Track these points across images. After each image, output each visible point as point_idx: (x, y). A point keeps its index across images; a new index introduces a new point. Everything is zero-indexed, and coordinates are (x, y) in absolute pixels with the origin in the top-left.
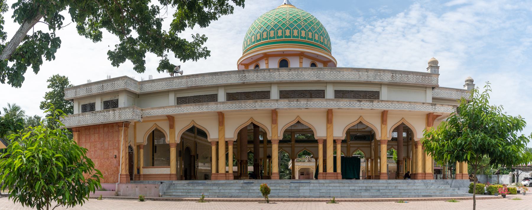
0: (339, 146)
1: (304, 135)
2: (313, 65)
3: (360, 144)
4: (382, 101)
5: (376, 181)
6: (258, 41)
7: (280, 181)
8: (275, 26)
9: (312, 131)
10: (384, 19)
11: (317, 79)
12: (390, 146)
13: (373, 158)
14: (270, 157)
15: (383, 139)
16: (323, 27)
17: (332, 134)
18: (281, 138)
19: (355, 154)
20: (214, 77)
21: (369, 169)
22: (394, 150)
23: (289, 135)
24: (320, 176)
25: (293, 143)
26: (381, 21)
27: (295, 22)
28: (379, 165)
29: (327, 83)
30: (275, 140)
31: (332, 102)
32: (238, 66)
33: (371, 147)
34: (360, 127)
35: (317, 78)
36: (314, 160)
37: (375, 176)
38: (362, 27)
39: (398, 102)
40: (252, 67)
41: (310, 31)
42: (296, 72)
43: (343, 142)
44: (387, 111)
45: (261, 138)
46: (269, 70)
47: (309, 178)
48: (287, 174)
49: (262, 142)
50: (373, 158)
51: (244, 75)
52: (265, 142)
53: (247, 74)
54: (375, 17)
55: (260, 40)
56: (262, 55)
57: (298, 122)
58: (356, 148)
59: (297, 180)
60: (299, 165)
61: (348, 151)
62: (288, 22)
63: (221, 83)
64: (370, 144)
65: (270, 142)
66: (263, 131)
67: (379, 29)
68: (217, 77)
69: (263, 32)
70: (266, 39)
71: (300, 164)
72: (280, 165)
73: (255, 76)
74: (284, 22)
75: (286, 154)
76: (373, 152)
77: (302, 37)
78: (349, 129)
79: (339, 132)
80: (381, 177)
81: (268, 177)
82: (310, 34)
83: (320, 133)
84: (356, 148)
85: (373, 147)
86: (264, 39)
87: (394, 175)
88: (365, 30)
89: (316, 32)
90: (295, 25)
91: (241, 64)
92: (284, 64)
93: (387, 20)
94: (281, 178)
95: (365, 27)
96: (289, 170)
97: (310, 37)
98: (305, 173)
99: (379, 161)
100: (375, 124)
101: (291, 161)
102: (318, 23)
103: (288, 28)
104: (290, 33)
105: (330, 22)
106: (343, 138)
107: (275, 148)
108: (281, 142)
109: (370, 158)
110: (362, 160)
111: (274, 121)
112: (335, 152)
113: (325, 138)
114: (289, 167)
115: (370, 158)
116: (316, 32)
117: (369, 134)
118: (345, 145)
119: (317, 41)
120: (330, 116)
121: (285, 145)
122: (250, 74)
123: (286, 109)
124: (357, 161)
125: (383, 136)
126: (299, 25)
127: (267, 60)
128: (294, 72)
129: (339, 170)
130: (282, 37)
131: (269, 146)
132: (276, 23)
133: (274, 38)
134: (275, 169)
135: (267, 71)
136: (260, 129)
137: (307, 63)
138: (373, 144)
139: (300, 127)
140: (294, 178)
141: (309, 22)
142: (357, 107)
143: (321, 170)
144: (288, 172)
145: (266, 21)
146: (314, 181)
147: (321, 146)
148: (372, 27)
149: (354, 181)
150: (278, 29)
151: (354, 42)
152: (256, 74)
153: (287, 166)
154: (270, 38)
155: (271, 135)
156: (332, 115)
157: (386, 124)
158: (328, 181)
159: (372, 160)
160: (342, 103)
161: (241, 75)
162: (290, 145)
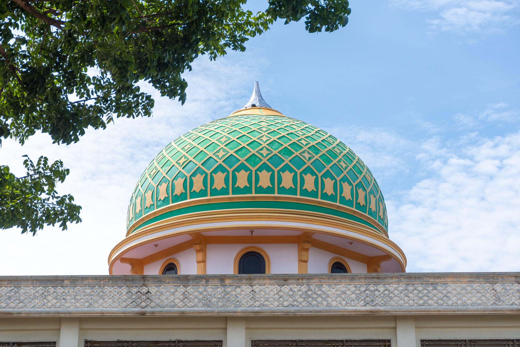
2: (338, 268)
6: (176, 198)
8: (229, 159)
10: (498, 138)
11: (368, 308)
16: (363, 166)
20: (52, 290)
26: (491, 143)
27: (287, 151)
29: (395, 319)
32: (111, 265)
35: (367, 304)
38: (437, 164)
40: (154, 270)
41: (328, 174)
42: (304, 288)
46: (310, 277)
51: (145, 290)
53: (153, 289)
54: (473, 135)
55: (183, 196)
56: (188, 238)
62: (264, 152)
63: (72, 309)
67: (487, 166)
68: (60, 290)
69: (194, 174)
70: (203, 193)
73: (178, 294)
74: (253, 152)
77: (305, 192)
82: (329, 183)
86: (194, 194)
88: (445, 171)
89: (344, 179)
90: (287, 160)
91: (122, 258)
92: (252, 264)
93: (507, 139)
95: (445, 162)
97: (329, 189)
102: (350, 156)
103: (265, 167)
104: (272, 179)
105: (374, 150)
116: (344, 179)
119: (350, 203)
122: (162, 289)
126: (298, 161)
127: (203, 250)
128: (295, 288)
130: (247, 190)
132: (232, 152)
133: (225, 191)
135: (216, 282)
137: (319, 263)
141: (324, 151)
145: (201, 148)
148: (467, 162)
150: (238, 169)
151: (416, 204)
152: (182, 289)
154: (214, 192)
161: (135, 290)
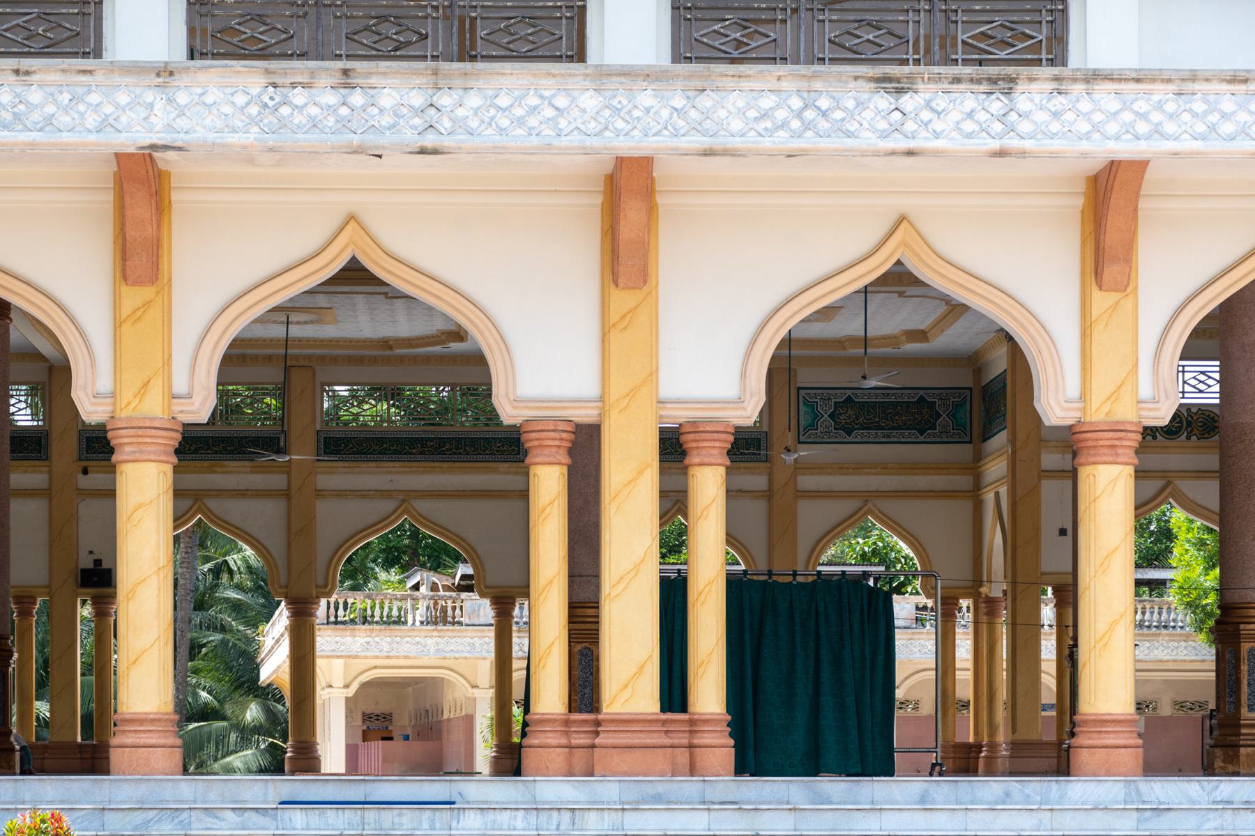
0: (709, 485)
1: (392, 393)
3: (883, 468)
4: (1093, 77)
5: (1035, 787)
7: (188, 789)
9: (478, 360)
12: (1156, 484)
13: (996, 589)
14: (99, 580)
15: (1097, 413)
17: (653, 375)
18: (200, 406)
19: (842, 556)
21: (964, 686)
22: (1178, 517)
23: (258, 390)
24: (543, 748)
25: (301, 455)
28: (1048, 648)
30: (142, 427)
31: (647, 98)
33: (975, 494)
34: (891, 319)
36: (480, 608)
37: (1017, 747)
39: (1237, 79)
43: (746, 447)
44: (1139, 167)
45: (23, 415)
47: (435, 766)
48: (247, 734)
49: (29, 445)
50: (996, 589)
52: (64, 449)
57: (354, 275)
58: (849, 506)
59: (334, 778)
60: (349, 658)
61: (780, 526)
64: (974, 468)
65: (97, 446)
66: (44, 347)
71: (358, 641)
72: (187, 650)
75: (234, 560)
76: (995, 541)
78: (788, 342)
79: (714, 367)
80: (1082, 757)
81: (89, 757)
83: (542, 367)
84: (849, 506)
85: (996, 493)
87: (1192, 741)
94: (196, 758)
96: (267, 694)
98: (403, 722)
99: (1048, 613)
100: (1023, 281)
101: (282, 618)
106: (748, 413)
107: (144, 497)
108: (195, 446)
109: (974, 588)
110: (903, 607)
111: (139, 256)
112: (673, 543)
113: (585, 415)
114: (265, 674)
115: (974, 588)
117: (964, 379)
118: (756, 480)
120: (632, 213)
121: (232, 475)
123: (246, 156)
124: (859, 614)
125: (1101, 387)
129: (709, 691)
131: (95, 480)
134: (145, 679)
136: (18, 332)
138: (996, 468)
139: (360, 322)
140: (307, 761)
142: (868, 140)
143: (551, 695)
144: (253, 713)
146: (486, 788)
147: (549, 483)
149: (833, 786)
153: (244, 677)
155: (104, 382)
156: (651, 208)
157: (1125, 284)
158: (609, 789)
159: (987, 609)
160: (736, 100)
162: (277, 481)
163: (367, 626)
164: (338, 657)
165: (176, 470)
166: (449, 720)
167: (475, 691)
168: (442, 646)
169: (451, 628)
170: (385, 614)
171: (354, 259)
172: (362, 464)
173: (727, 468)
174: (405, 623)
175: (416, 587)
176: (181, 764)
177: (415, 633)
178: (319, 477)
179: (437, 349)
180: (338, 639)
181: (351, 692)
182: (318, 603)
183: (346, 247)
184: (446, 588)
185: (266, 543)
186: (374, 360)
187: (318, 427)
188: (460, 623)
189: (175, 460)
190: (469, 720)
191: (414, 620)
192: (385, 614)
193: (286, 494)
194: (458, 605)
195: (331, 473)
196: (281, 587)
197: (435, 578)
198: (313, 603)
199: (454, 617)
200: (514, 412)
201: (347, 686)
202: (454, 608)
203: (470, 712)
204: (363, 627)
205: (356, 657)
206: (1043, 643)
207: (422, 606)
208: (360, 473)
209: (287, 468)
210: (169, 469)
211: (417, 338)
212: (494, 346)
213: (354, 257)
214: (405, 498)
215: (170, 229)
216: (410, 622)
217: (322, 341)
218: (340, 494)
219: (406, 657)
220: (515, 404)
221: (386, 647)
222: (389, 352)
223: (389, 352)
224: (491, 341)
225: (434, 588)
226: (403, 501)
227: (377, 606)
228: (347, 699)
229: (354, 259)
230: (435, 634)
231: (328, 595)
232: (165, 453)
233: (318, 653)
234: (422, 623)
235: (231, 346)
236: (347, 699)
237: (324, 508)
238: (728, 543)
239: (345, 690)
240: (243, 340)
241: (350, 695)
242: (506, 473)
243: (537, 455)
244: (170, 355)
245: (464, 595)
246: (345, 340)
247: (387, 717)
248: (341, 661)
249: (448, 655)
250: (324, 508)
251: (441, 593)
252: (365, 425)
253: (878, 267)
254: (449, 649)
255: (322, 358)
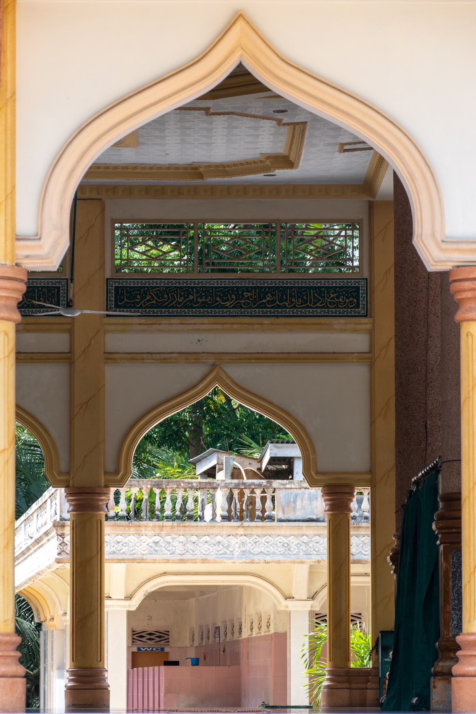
98: (182, 643)
163: (155, 523)
164: (119, 561)
165: (20, 329)
166: (248, 640)
167: (289, 603)
168: (248, 547)
169: (261, 524)
170: (178, 506)
171: (240, 66)
172: (164, 321)
173: (17, 325)
174: (202, 518)
175: (211, 473)
176: (24, 698)
177: (214, 531)
178: (109, 337)
179: (259, 177)
180: (119, 538)
181: (134, 605)
182: (107, 494)
183: (232, 52)
184: (251, 474)
185: (43, 419)
186: (178, 192)
187: (108, 275)
188: (271, 518)
189: (17, 316)
190: (281, 641)
191: (214, 515)
192: (178, 506)
193: (67, 358)
194: (269, 496)
195: (124, 331)
196: (60, 473)
197: (236, 462)
198: (100, 494)
199: (263, 511)
200: (442, 256)
201: (129, 598)
202: (263, 500)
203: (281, 630)
204: (151, 523)
205: (142, 561)
206: (353, 540)
207: (220, 496)
208: (160, 331)
209: (70, 327)
210: (10, 328)
211: (235, 164)
212: (417, 175)
213: (240, 66)
214: (217, 361)
215: (14, 30)
216: (208, 516)
217: (116, 167)
218: (135, 357)
219: (204, 561)
220: (444, 246)
221: (179, 549)
222: (197, 182)
223: (197, 182)
224: (413, 168)
225: (235, 474)
226: (214, 366)
227: (168, 500)
228: (129, 613)
229: (240, 66)
230: (241, 531)
231: (120, 483)
232: (7, 308)
233: (106, 556)
234: (224, 518)
235: (88, 175)
236: (129, 613)
237: (115, 376)
238: (18, 416)
239: (127, 603)
240: (107, 167)
241: (133, 609)
242: (342, 331)
243: (471, 310)
244: (14, 187)
245: (276, 483)
246: (144, 167)
247: (162, 636)
248: (123, 566)
249: (256, 558)
250: (115, 376)
251: (245, 480)
252: (138, 271)
253: (226, 71)
254: (257, 550)
255: (113, 189)
